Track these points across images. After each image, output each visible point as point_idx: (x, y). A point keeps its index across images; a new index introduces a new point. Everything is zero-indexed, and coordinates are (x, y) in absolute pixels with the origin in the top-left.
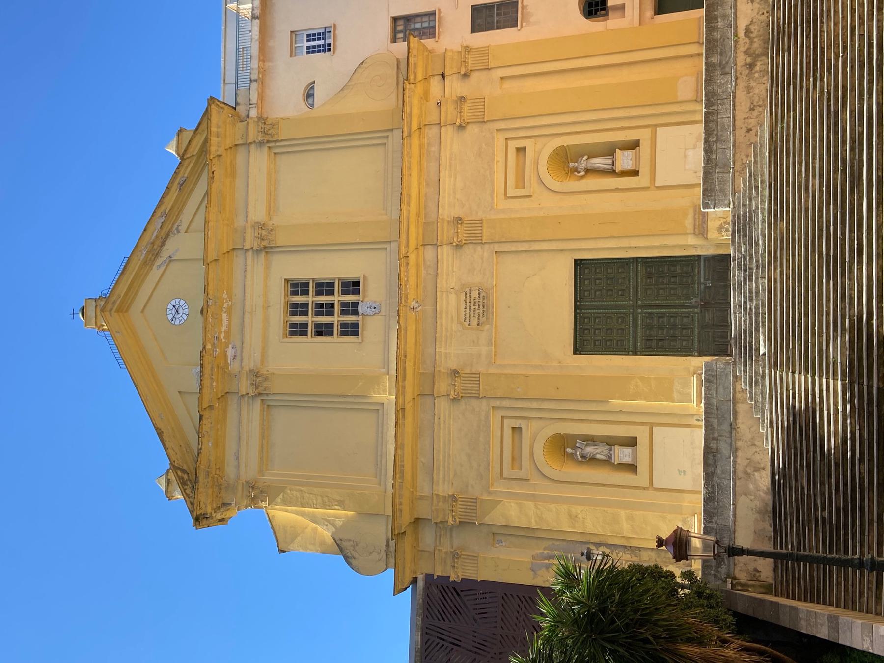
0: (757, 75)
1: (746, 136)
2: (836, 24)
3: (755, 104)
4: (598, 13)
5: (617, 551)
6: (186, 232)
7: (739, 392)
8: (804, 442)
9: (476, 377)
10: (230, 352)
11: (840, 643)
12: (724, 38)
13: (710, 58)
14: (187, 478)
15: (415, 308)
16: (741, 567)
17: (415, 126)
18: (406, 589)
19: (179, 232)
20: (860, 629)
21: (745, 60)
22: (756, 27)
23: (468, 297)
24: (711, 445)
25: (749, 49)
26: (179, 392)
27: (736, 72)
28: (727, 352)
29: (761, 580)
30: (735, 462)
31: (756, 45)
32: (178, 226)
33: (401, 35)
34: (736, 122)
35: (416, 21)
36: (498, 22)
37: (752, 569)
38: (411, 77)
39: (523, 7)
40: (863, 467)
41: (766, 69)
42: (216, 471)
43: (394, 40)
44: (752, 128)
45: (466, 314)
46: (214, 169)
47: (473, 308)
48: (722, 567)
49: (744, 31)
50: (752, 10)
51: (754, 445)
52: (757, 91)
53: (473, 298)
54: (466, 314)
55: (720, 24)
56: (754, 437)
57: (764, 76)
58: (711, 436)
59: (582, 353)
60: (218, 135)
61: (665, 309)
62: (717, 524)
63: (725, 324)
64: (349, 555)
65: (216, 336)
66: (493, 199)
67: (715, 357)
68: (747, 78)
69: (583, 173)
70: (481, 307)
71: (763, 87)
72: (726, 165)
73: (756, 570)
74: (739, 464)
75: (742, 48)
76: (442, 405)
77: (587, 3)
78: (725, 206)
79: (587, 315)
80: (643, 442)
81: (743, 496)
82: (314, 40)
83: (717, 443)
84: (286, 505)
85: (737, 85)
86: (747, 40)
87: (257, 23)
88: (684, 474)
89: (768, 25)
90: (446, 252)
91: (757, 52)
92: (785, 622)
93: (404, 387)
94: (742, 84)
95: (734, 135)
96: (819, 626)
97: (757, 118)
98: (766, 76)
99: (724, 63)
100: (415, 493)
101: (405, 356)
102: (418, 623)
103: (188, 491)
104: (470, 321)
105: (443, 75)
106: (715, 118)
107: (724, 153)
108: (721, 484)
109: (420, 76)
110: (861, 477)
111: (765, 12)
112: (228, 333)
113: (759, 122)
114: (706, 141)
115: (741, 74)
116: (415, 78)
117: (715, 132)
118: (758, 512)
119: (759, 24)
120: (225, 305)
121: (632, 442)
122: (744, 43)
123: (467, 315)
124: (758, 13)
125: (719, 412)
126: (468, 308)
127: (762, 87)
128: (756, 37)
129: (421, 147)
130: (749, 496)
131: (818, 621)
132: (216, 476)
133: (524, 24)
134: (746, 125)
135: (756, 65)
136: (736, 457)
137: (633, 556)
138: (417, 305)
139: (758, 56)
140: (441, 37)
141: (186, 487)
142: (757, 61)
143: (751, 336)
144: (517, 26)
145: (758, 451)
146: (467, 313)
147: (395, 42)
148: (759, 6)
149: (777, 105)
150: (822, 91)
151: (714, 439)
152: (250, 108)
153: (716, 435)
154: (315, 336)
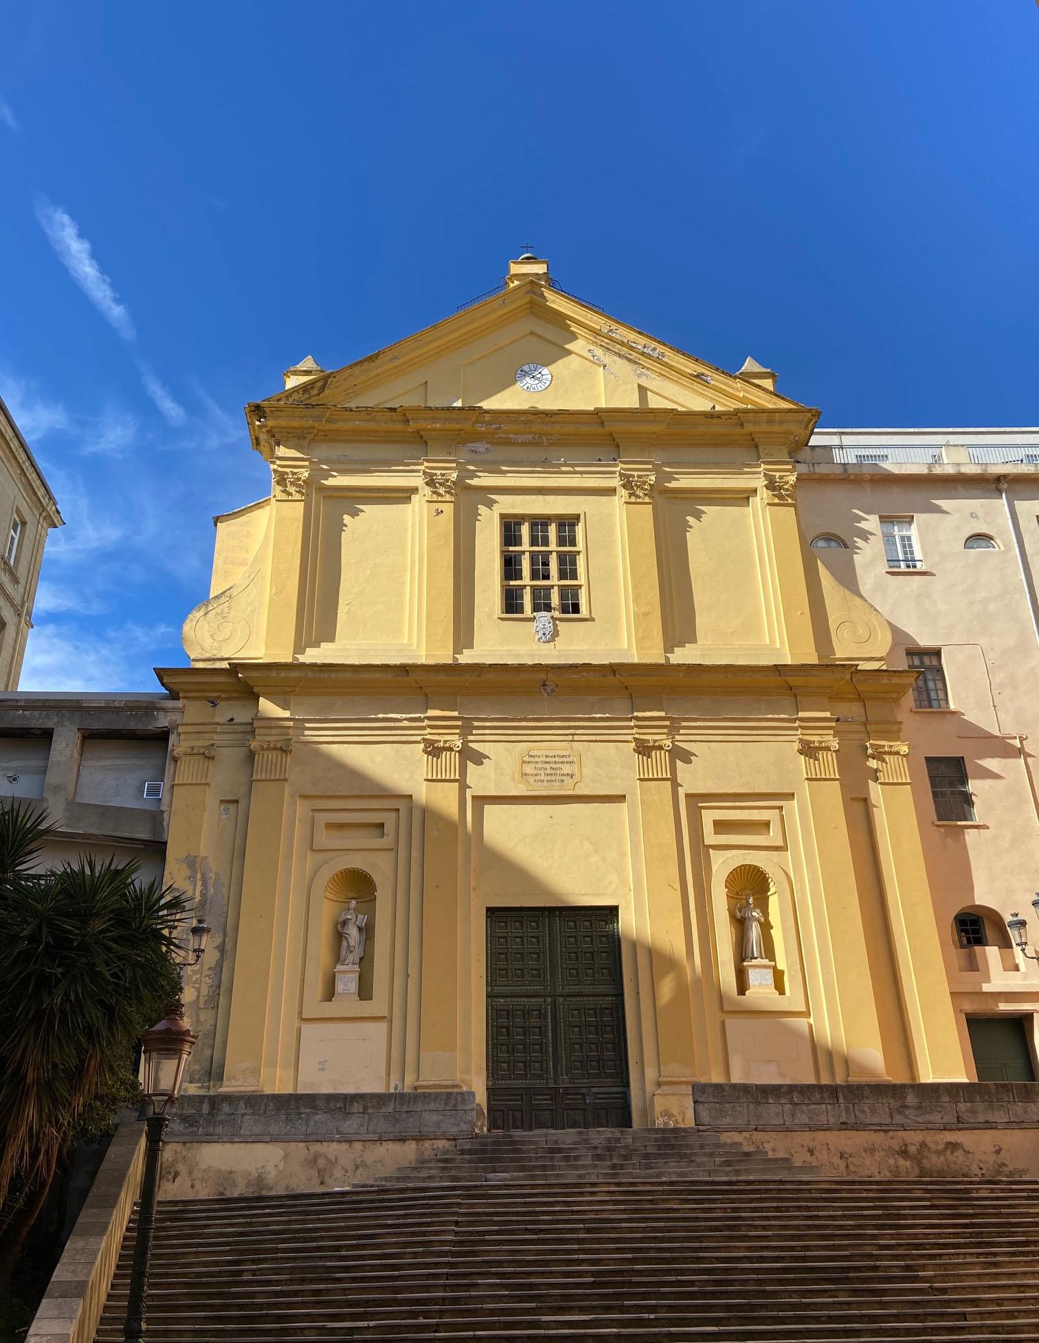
0: (892, 1161)
1: (803, 1147)
2: (979, 1276)
3: (850, 1160)
4: (963, 934)
5: (213, 975)
7: (433, 1145)
8: (355, 1242)
11: (44, 1301)
13: (913, 1091)
14: (314, 394)
15: (546, 688)
16: (181, 1153)
18: (163, 685)
19: (638, 377)
20: (58, 1331)
21: (911, 1144)
22: (961, 1159)
23: (561, 760)
24: (356, 1104)
25: (929, 1148)
26: (427, 382)
28: (494, 1128)
29: (161, 1183)
31: (934, 1158)
32: (647, 375)
33: (917, 662)
34: (822, 1132)
35: (937, 682)
36: (943, 794)
37: (177, 1168)
40: (313, 1334)
41: (901, 1175)
42: (322, 431)
44: (814, 1157)
45: (539, 757)
47: (548, 766)
48: (182, 1124)
49: (954, 1142)
50: (985, 1153)
51: (357, 1167)
52: (868, 1162)
53: (558, 766)
54: (539, 757)
55: (962, 1106)
56: (368, 1168)
57: (890, 1171)
58: (369, 1105)
59: (489, 919)
61: (552, 1037)
62: (243, 1116)
63: (534, 1124)
65: (502, 426)
67: (485, 1111)
68: (886, 1148)
70: (549, 778)
71: (874, 1170)
73: (176, 1175)
74: (329, 1146)
77: (976, 918)
79: (540, 924)
80: (368, 1008)
81: (282, 1153)
83: (359, 1113)
84: (277, 522)
85: (875, 1132)
86: (941, 1147)
87: (923, 471)
88: (320, 1069)
89: (964, 1176)
91: (925, 1161)
92: (86, 1216)
96: (72, 1268)
97: (830, 1163)
98: (890, 1174)
99: (907, 1112)
100: (293, 694)
102: (116, 703)
103: (295, 396)
104: (529, 762)
106: (827, 1101)
108: (300, 1121)
110: (298, 1331)
111: (983, 1172)
113: (824, 1167)
114: (792, 1088)
115: (892, 1138)
117: (806, 1101)
118: (259, 1176)
119: (966, 1163)
121: (365, 992)
122: (937, 1142)
123: (537, 759)
124: (981, 1161)
125: (404, 1115)
126: (548, 760)
127: (874, 1167)
128: (946, 1160)
130: (283, 1162)
131: (81, 1267)
132: (315, 431)
133: (942, 830)
134: (819, 1147)
135: (906, 1160)
137: (206, 998)
139: (919, 1163)
140: (917, 716)
142: (912, 1162)
143: (512, 1160)
144: (939, 820)
145: (349, 1174)
146: (541, 759)
147: (908, 654)
148: (992, 1162)
149: (850, 1191)
150: (878, 1257)
151: (366, 1108)
152: (808, 464)
153: (370, 1111)
154: (505, 555)
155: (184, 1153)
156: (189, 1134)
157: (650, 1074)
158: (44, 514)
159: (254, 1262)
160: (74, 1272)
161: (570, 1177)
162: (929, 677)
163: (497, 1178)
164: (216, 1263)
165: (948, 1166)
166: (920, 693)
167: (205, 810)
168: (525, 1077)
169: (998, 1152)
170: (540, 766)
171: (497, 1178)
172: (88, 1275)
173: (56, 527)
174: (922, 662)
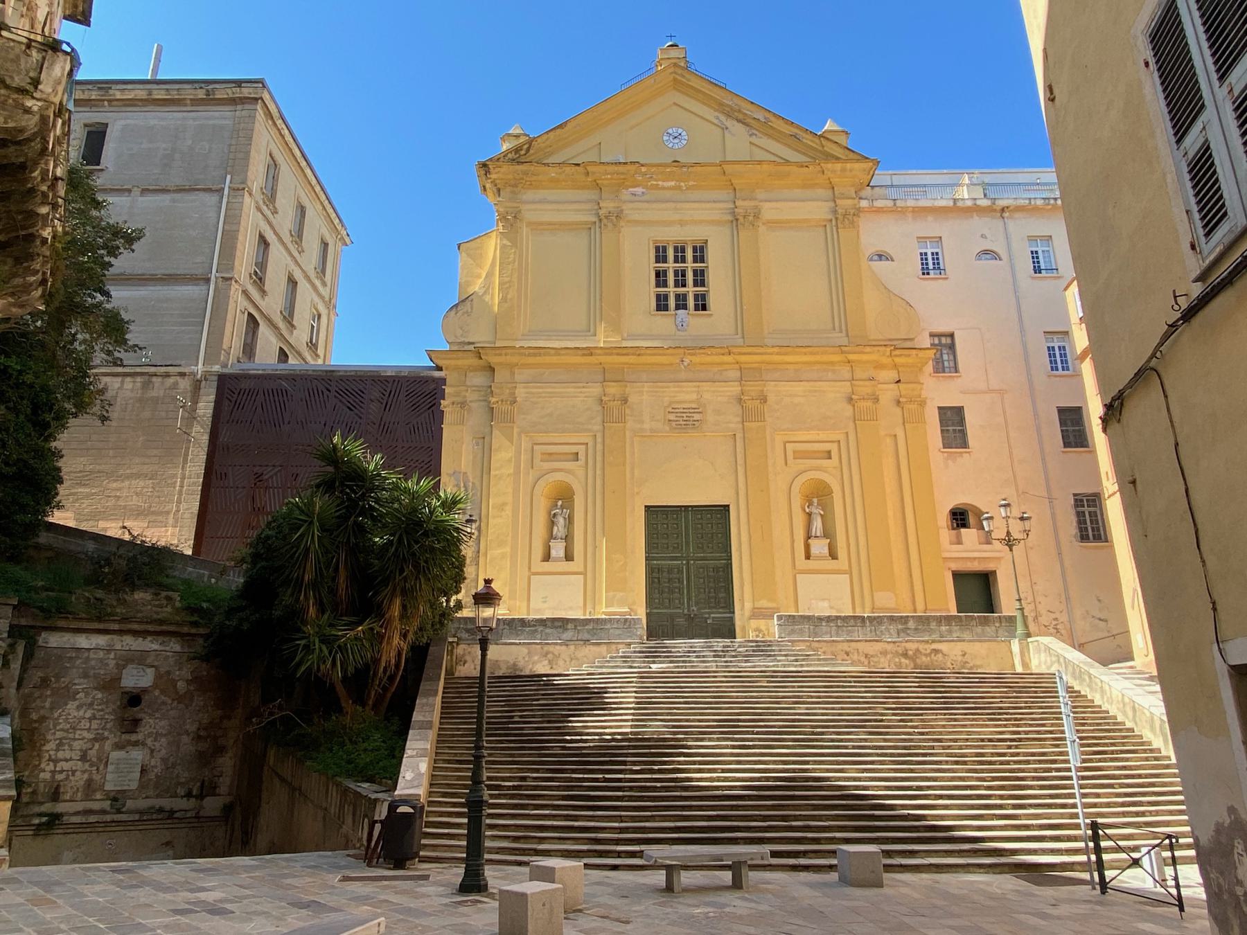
0: (897, 660)
2: (944, 726)
6: (750, 143)
9: (622, 419)
10: (639, 190)
12: (931, 632)
17: (851, 357)
27: (901, 642)
30: (556, 644)
31: (924, 658)
33: (936, 341)
38: (898, 352)
39: (961, 453)
43: (932, 335)
46: (811, 167)
47: (684, 415)
51: (572, 659)
52: (882, 660)
60: (843, 170)
64: (459, 308)
66: (784, 430)
69: (807, 510)
72: (816, 635)
75: (921, 647)
76: (596, 390)
78: (780, 634)
82: (933, 259)
86: (928, 651)
90: (735, 389)
91: (917, 660)
92: (423, 686)
93: (611, 354)
94: (889, 647)
95: (843, 641)
101: (639, 355)
105: (899, 381)
107: (826, 633)
109: (897, 360)
112: (657, 187)
115: (898, 646)
116: (896, 356)
120: (682, 184)
121: (569, 557)
123: (677, 410)
129: (832, 363)
133: (946, 455)
136: (561, 644)
138: (685, 364)
140: (934, 379)
141: (513, 153)
151: (576, 626)
155: (469, 650)
156: (472, 640)
157: (748, 605)
158: (339, 237)
159: (520, 711)
160: (424, 716)
161: (701, 667)
162: (945, 352)
163: (654, 667)
164: (498, 712)
165: (932, 664)
166: (937, 363)
167: (463, 443)
168: (669, 608)
169: (964, 655)
170: (679, 415)
171: (654, 667)
172: (432, 718)
173: (347, 245)
174: (940, 340)
